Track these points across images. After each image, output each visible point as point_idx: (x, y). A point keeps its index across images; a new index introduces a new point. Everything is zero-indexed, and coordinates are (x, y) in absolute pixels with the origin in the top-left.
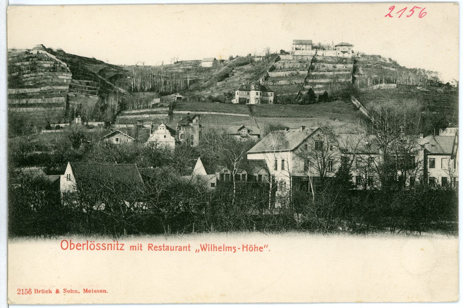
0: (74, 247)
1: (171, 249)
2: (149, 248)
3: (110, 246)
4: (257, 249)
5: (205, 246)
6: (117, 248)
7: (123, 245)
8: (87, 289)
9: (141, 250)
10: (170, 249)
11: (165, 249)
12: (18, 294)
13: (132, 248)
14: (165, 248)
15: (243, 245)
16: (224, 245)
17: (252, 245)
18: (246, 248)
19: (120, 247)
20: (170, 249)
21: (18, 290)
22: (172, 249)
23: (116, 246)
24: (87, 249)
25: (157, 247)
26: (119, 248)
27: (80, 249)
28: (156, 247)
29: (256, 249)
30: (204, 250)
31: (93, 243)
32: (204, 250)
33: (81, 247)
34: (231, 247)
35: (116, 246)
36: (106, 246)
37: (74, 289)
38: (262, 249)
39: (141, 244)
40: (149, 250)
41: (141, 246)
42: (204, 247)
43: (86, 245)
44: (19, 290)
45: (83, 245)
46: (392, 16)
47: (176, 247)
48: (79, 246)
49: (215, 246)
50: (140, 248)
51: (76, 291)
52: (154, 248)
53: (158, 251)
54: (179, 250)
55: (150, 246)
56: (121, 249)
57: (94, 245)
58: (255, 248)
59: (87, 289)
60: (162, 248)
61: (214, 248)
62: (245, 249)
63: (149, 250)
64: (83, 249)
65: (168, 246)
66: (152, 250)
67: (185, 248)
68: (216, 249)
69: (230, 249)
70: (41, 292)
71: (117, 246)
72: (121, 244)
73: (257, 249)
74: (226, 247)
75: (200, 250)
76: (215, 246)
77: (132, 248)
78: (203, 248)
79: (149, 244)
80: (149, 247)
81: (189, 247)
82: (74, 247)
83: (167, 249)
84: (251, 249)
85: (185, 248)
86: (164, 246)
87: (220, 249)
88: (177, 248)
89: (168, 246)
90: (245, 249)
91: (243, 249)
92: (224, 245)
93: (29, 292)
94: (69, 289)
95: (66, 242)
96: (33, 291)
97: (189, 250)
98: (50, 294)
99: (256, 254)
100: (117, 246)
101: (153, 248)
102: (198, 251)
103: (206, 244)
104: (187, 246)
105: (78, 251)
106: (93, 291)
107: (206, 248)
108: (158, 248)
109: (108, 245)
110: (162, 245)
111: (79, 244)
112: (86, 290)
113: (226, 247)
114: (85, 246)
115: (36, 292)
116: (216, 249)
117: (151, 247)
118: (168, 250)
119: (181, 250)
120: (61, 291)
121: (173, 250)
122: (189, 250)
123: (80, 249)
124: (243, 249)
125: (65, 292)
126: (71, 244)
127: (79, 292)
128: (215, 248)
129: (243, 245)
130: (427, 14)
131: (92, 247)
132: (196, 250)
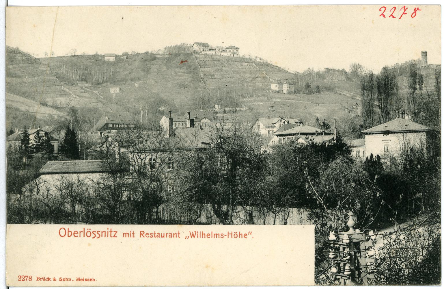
0: (71, 235)
1: (176, 235)
2: (141, 235)
3: (104, 233)
4: (242, 236)
5: (194, 234)
6: (111, 235)
7: (116, 232)
8: (79, 278)
9: (179, 237)
10: (160, 236)
11: (156, 236)
12: (19, 280)
13: (125, 235)
14: (156, 235)
15: (228, 232)
16: (212, 232)
17: (237, 232)
18: (231, 235)
19: (113, 234)
20: (160, 236)
21: (19, 277)
22: (175, 235)
23: (109, 233)
24: (84, 236)
25: (149, 235)
26: (113, 235)
27: (77, 236)
28: (147, 234)
29: (241, 235)
30: (193, 237)
31: (90, 230)
32: (193, 237)
33: (78, 235)
34: (219, 234)
35: (109, 233)
36: (100, 233)
37: (68, 278)
38: (247, 235)
39: (133, 232)
40: (141, 237)
41: (133, 233)
42: (193, 234)
43: (83, 232)
44: (20, 277)
45: (80, 232)
46: (395, 16)
47: (167, 234)
48: (76, 233)
49: (203, 233)
50: (132, 235)
51: (70, 280)
52: (146, 235)
53: (149, 238)
54: (169, 237)
55: (142, 233)
56: (114, 236)
57: (90, 232)
58: (240, 235)
59: (79, 278)
60: (153, 235)
61: (203, 235)
62: (230, 236)
63: (141, 237)
64: (80, 236)
65: (159, 234)
66: (144, 237)
67: (175, 235)
68: (205, 236)
69: (218, 235)
70: (42, 280)
71: (111, 234)
72: (114, 232)
73: (242, 236)
74: (214, 234)
75: (190, 237)
76: (203, 233)
77: (125, 234)
78: (193, 235)
79: (141, 231)
80: (141, 234)
81: (179, 234)
82: (71, 235)
83: (170, 236)
84: (236, 236)
85: (163, 236)
86: (155, 234)
87: (208, 236)
88: (168, 235)
89: (159, 234)
90: (230, 236)
91: (228, 235)
92: (212, 232)
93: (49, 279)
94: (64, 277)
95: (64, 231)
96: (34, 278)
97: (133, 237)
98: (49, 281)
99: (241, 240)
100: (111, 234)
101: (144, 235)
102: (187, 237)
103: (195, 232)
104: (177, 233)
105: (63, 238)
106: (85, 280)
107: (195, 235)
108: (150, 235)
109: (102, 232)
110: (153, 232)
111: (76, 231)
112: (78, 279)
113: (214, 234)
114: (82, 234)
115: (38, 279)
116: (205, 236)
117: (142, 234)
118: (159, 237)
119: (171, 237)
120: (58, 279)
121: (164, 237)
122: (179, 237)
123: (77, 236)
124: (228, 235)
125: (61, 280)
126: (68, 232)
127: (73, 281)
128: (204, 235)
129: (228, 232)
130: (379, 9)
131: (89, 234)
132: (186, 237)
